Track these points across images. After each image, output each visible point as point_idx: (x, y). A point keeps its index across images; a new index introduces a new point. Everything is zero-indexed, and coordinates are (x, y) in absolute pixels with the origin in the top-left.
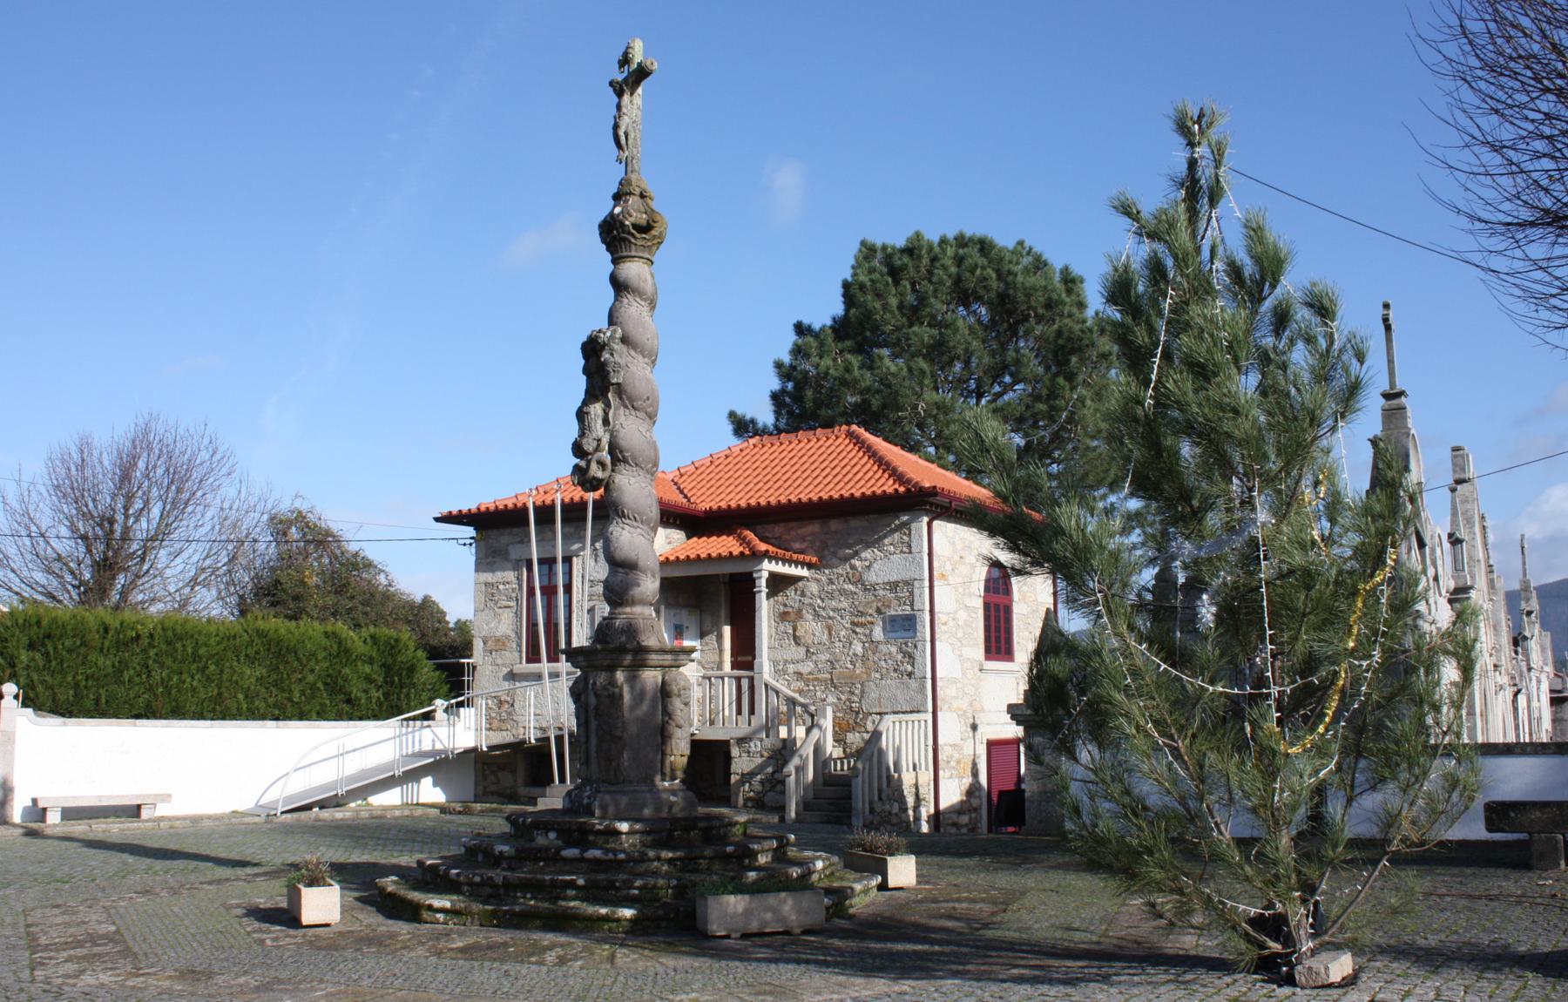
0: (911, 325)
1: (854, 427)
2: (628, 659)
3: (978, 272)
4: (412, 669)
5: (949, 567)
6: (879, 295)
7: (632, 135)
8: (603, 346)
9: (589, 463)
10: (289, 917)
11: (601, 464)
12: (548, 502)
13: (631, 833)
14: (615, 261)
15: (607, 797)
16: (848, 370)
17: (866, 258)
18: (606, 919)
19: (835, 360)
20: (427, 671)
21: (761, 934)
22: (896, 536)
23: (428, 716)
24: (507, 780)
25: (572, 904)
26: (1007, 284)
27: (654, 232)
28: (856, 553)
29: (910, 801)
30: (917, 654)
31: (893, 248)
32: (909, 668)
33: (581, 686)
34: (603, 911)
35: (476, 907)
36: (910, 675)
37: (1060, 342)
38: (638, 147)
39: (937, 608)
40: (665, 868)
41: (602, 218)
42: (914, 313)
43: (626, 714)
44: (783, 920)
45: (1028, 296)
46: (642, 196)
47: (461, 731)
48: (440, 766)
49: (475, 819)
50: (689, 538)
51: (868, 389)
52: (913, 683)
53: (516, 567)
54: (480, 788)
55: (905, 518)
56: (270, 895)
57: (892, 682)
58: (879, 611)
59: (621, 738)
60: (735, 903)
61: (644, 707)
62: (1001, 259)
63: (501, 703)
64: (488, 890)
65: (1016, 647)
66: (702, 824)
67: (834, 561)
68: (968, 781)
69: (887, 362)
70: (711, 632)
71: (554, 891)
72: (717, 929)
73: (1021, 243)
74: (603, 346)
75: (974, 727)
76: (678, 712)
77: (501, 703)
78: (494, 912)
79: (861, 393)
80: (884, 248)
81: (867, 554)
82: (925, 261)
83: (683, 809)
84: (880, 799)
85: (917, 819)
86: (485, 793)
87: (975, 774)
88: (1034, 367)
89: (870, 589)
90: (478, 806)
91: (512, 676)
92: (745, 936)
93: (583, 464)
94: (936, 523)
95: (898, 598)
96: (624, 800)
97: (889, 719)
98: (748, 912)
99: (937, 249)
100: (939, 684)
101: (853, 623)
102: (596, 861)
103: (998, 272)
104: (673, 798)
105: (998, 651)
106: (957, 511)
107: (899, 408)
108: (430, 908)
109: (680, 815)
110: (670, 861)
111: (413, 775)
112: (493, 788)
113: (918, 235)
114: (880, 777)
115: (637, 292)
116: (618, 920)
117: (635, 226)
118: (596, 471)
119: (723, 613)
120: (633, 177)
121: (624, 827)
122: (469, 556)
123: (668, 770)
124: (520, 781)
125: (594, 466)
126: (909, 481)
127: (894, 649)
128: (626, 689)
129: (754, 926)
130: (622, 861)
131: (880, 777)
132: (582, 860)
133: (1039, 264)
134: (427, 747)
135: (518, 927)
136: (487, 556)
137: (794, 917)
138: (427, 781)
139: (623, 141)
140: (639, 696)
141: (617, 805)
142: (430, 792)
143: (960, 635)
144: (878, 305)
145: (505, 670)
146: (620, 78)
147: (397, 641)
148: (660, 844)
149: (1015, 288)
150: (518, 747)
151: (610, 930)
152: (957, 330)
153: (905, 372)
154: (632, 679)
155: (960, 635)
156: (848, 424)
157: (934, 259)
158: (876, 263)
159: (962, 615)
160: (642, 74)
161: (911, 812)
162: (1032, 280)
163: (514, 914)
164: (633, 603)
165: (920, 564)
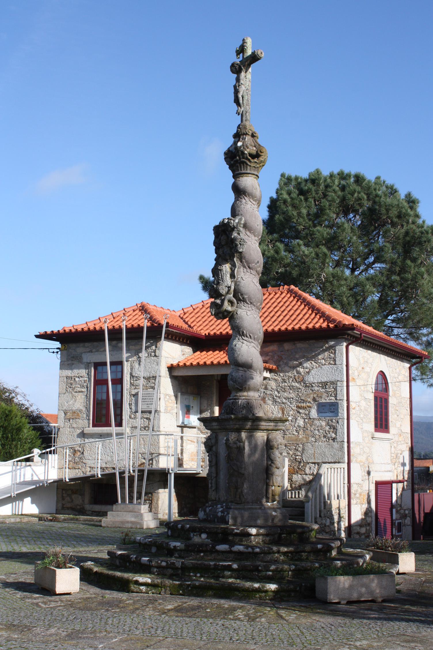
0: (315, 226)
1: (292, 287)
2: (249, 424)
3: (356, 195)
4: (19, 430)
5: (356, 374)
6: (294, 207)
7: (246, 98)
8: (233, 229)
9: (223, 301)
10: (45, 588)
11: (231, 302)
12: (117, 327)
13: (257, 535)
14: (235, 176)
15: (236, 512)
16: (277, 252)
17: (285, 184)
18: (258, 590)
19: (268, 245)
20: (27, 432)
21: (358, 602)
22: (326, 354)
23: (28, 460)
24: (78, 500)
25: (230, 580)
26: (374, 202)
27: (261, 159)
28: (301, 364)
29: (336, 518)
30: (339, 427)
31: (301, 179)
32: (333, 435)
33: (213, 441)
34: (256, 585)
35: (168, 582)
36: (334, 439)
37: (408, 239)
38: (248, 105)
39: (351, 399)
40: (282, 558)
41: (225, 149)
42: (317, 217)
43: (246, 459)
44: (371, 593)
45: (387, 210)
46: (253, 136)
47: (48, 469)
48: (37, 491)
49: (59, 525)
50: (194, 352)
51: (288, 265)
52: (336, 445)
53: (87, 366)
54: (60, 505)
55: (333, 343)
56: (25, 573)
57: (322, 444)
58: (314, 400)
59: (243, 474)
60: (344, 581)
61: (257, 455)
62: (369, 188)
63: (75, 451)
64: (170, 571)
65: (391, 424)
66: (299, 530)
67: (287, 368)
68: (365, 506)
69: (303, 248)
70: (207, 410)
71: (216, 572)
72: (333, 598)
73: (378, 178)
74: (233, 229)
75: (369, 473)
76: (278, 459)
77: (75, 451)
78: (180, 586)
79: (284, 266)
80: (296, 178)
81: (307, 365)
82: (322, 187)
83: (280, 520)
84: (320, 516)
85: (339, 529)
86: (63, 508)
87: (369, 502)
88: (390, 254)
89: (309, 386)
90: (61, 517)
91: (83, 435)
92: (349, 603)
93: (218, 301)
94: (351, 347)
95: (327, 392)
96: (246, 514)
97: (325, 467)
98: (351, 587)
99: (329, 180)
100: (351, 445)
101: (298, 407)
102: (240, 553)
103: (368, 195)
104: (274, 513)
105: (381, 427)
106: (364, 340)
107: (308, 276)
108: (137, 583)
109: (279, 524)
110: (285, 554)
111: (21, 497)
112: (69, 505)
113: (318, 172)
114: (320, 502)
115: (251, 196)
116: (266, 591)
117: (250, 155)
118: (227, 306)
119: (215, 398)
120: (247, 124)
121: (254, 531)
122: (56, 359)
123: (270, 496)
124: (87, 500)
125: (226, 303)
126: (334, 321)
127: (324, 424)
128: (247, 444)
129: (355, 596)
130: (257, 553)
131: (320, 502)
132: (231, 552)
133: (392, 191)
134: (28, 478)
135: (197, 595)
136: (68, 360)
137: (378, 591)
138: (28, 500)
139: (241, 101)
140: (254, 448)
141: (242, 517)
142: (29, 507)
143: (362, 416)
144: (295, 213)
145: (79, 431)
146: (238, 61)
147: (10, 411)
148: (279, 542)
149: (380, 206)
150: (85, 480)
151: (260, 598)
152: (344, 230)
153: (313, 255)
154: (250, 437)
155: (362, 416)
156: (289, 285)
157: (327, 186)
158: (291, 187)
159: (363, 404)
160: (255, 58)
161: (336, 525)
162: (389, 200)
163: (195, 587)
164: (249, 390)
165: (341, 371)
